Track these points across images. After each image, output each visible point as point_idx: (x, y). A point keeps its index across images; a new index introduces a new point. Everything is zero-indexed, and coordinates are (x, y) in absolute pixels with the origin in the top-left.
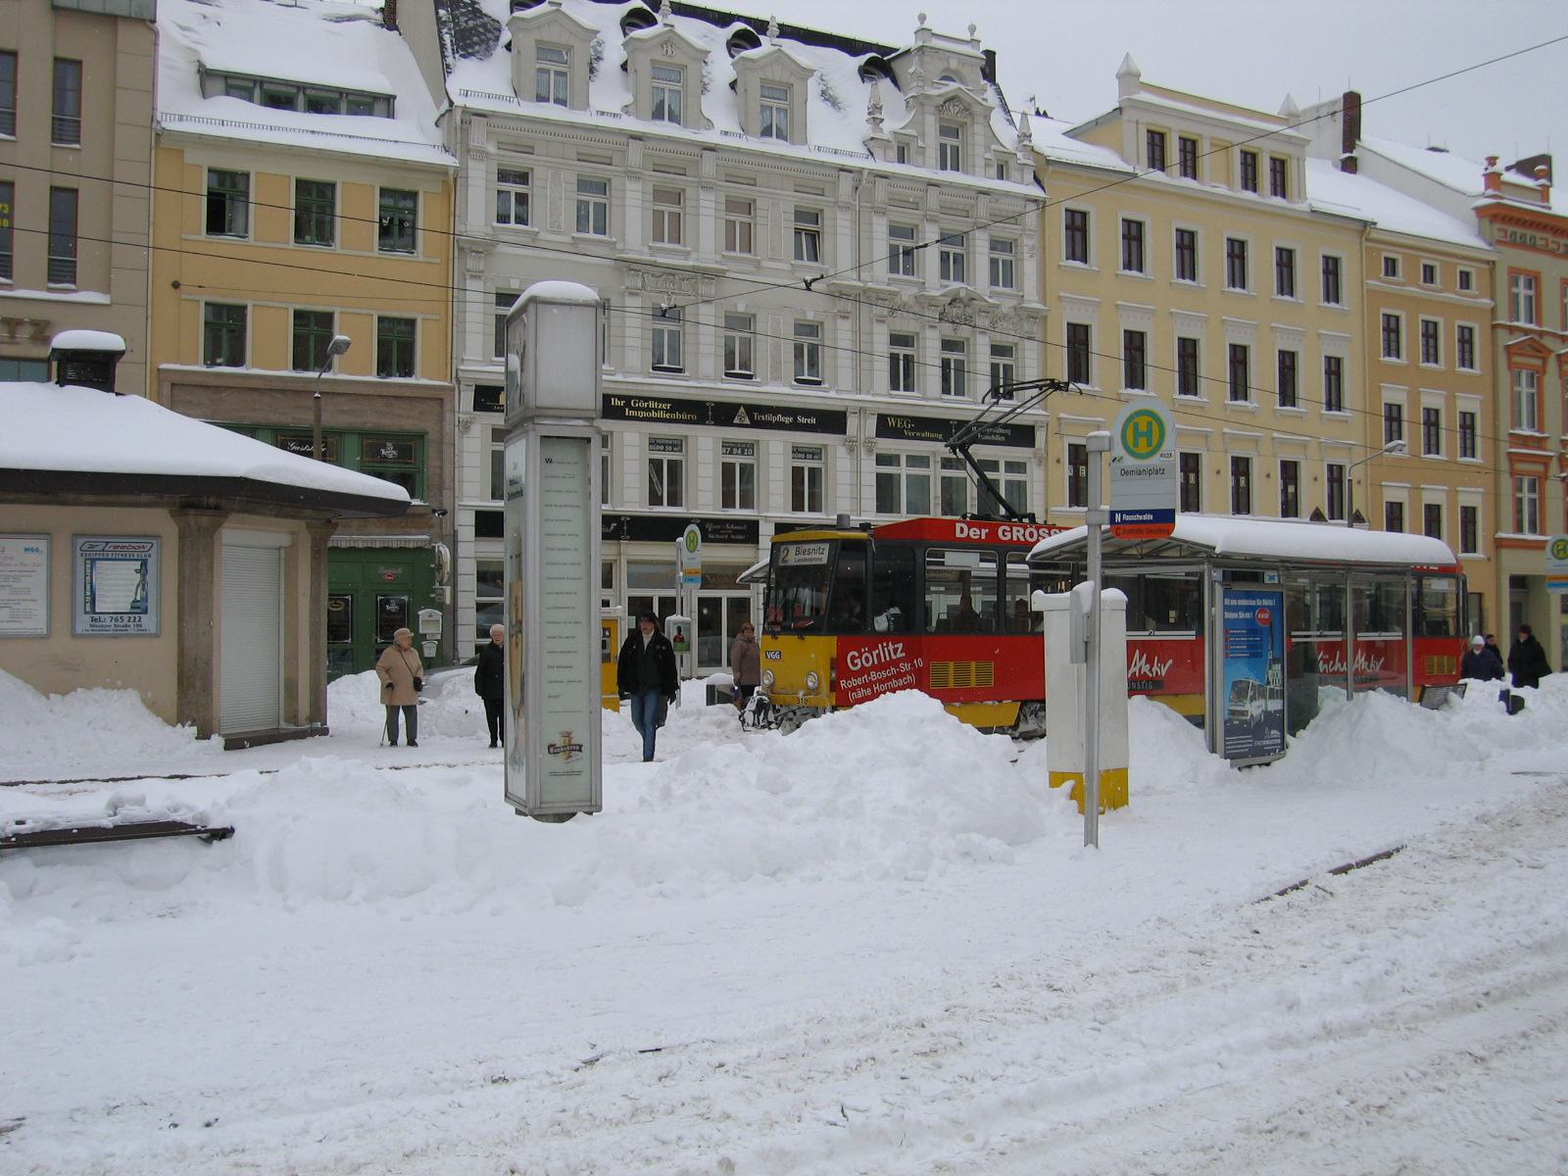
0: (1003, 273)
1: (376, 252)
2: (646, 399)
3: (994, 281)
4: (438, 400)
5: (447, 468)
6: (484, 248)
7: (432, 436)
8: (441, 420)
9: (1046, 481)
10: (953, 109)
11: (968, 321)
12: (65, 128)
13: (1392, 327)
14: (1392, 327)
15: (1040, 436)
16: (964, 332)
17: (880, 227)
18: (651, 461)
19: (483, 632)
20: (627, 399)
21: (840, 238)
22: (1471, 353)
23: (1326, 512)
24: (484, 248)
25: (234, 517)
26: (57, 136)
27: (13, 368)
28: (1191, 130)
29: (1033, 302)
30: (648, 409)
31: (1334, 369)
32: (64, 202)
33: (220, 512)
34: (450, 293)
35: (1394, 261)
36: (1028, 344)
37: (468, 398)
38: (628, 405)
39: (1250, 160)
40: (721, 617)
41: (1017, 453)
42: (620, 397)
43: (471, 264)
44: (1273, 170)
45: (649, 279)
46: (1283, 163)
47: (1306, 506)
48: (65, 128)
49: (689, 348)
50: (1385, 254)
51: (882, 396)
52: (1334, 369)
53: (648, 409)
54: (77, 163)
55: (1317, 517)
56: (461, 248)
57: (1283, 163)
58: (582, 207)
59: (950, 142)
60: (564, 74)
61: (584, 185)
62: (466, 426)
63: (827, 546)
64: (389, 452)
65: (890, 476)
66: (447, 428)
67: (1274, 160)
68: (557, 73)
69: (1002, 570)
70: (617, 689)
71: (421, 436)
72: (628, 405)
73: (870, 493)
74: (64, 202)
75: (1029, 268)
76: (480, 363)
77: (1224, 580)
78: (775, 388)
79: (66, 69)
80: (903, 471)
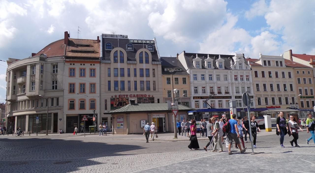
7: (189, 102)
8: (190, 100)
12: (154, 75)
13: (299, 80)
14: (299, 80)
19: (11, 113)
21: (192, 87)
22: (300, 81)
23: (292, 103)
26: (149, 82)
27: (312, 57)
28: (269, 60)
31: (291, 86)
34: (190, 87)
39: (277, 62)
44: (280, 63)
46: (281, 62)
47: (289, 103)
49: (229, 90)
51: (235, 94)
52: (291, 86)
54: (155, 79)
55: (291, 104)
57: (281, 62)
58: (202, 77)
63: (238, 113)
64: (185, 104)
65: (240, 103)
67: (280, 61)
69: (256, 113)
70: (299, 134)
71: (188, 102)
76: (193, 95)
77: (49, 114)
78: (223, 94)
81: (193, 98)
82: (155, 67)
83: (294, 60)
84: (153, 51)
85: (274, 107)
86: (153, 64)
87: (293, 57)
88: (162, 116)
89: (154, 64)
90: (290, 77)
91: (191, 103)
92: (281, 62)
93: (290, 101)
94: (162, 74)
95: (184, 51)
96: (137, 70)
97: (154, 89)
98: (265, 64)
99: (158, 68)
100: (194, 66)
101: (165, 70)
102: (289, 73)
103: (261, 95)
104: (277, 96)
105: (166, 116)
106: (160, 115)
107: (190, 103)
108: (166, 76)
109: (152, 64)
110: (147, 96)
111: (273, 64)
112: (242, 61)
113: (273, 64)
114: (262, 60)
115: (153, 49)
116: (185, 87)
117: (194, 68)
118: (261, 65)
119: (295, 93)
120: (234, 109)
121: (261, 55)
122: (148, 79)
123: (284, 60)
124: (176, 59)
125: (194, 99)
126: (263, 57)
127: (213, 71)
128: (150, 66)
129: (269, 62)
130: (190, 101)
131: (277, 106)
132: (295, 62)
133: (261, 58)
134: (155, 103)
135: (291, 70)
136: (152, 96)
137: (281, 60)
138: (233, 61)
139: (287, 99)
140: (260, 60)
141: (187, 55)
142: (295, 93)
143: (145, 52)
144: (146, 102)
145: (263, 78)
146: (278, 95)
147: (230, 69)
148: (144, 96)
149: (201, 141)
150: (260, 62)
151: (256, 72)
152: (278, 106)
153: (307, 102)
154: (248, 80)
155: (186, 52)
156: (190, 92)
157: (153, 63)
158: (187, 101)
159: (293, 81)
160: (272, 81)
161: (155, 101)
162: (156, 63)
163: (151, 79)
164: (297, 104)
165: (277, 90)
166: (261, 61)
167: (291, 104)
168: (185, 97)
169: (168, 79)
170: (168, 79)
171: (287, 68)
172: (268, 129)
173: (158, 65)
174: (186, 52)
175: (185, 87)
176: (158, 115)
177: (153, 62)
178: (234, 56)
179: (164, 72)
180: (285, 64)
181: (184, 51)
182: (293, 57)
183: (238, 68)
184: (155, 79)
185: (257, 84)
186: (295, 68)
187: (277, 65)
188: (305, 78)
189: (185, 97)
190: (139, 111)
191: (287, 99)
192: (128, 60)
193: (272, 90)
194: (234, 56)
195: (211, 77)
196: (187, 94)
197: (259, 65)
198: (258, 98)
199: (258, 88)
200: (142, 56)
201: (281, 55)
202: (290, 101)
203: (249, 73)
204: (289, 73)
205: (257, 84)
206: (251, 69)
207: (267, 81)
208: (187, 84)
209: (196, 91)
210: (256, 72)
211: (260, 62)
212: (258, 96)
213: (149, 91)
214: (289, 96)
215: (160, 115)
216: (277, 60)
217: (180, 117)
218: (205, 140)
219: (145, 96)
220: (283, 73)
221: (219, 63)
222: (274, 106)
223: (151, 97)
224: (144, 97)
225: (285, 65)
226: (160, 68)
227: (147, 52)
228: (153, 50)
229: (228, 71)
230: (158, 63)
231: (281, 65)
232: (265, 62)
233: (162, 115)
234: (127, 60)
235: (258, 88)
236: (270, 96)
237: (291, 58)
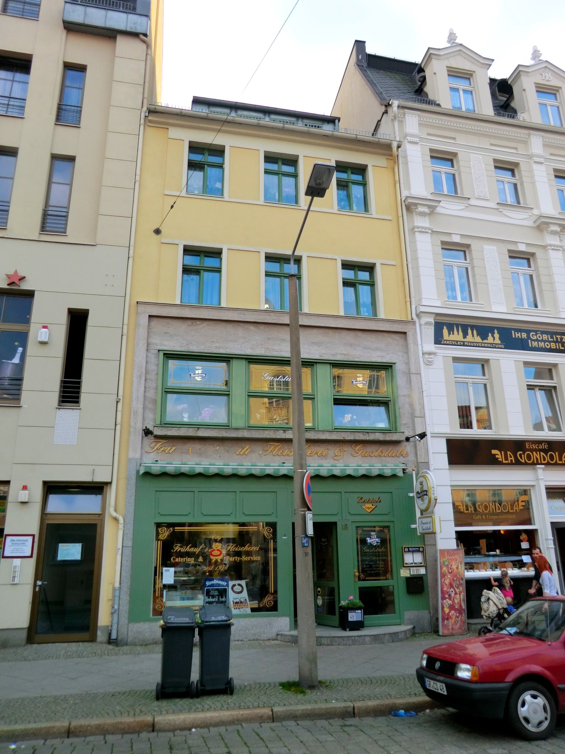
7: (399, 367)
38: (533, 336)
48: (67, 114)
81: (430, 332)
107: (408, 374)
125: (439, 340)
130: (408, 363)
161: (33, 327)
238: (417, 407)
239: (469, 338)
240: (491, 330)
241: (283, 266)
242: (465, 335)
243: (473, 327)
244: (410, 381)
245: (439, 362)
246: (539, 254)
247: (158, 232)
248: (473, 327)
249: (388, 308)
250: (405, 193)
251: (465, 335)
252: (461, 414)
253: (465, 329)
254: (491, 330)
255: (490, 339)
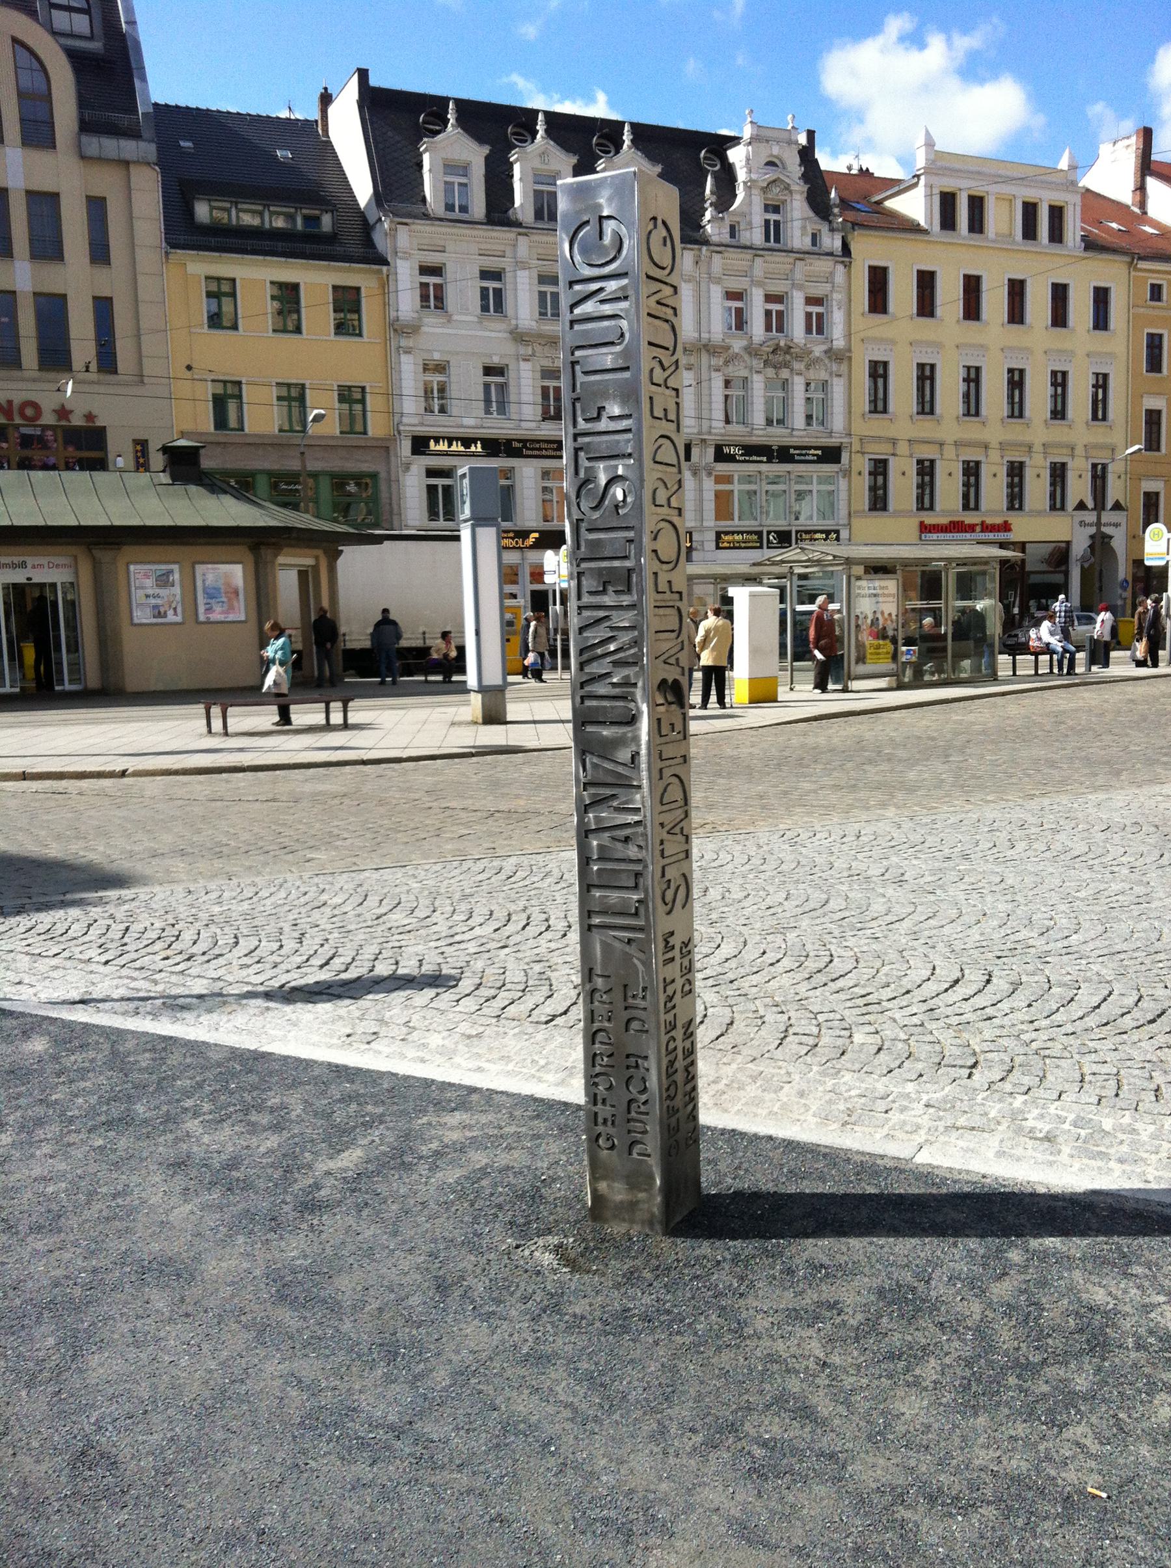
0: (817, 324)
1: (332, 337)
2: (538, 441)
3: (809, 330)
4: (385, 448)
5: (394, 498)
6: (413, 329)
7: (383, 475)
8: (388, 462)
9: (849, 490)
10: (776, 190)
11: (786, 365)
12: (100, 253)
15: (845, 457)
16: (785, 373)
17: (717, 292)
18: (540, 292)
20: (524, 441)
23: (1090, 505)
24: (413, 329)
25: (285, 550)
29: (839, 343)
30: (540, 449)
32: (103, 308)
33: (278, 548)
35: (1159, 287)
36: (836, 380)
37: (406, 446)
38: (525, 446)
40: (461, 593)
41: (828, 468)
42: (519, 441)
43: (404, 343)
45: (538, 348)
47: (1071, 503)
48: (100, 253)
50: (1150, 281)
52: (1101, 382)
53: (540, 449)
54: (111, 282)
55: (1081, 506)
56: (399, 329)
57: (981, 199)
58: (484, 292)
59: (773, 217)
60: (465, 185)
61: (485, 275)
62: (407, 467)
66: (393, 469)
68: (460, 184)
71: (374, 476)
72: (525, 446)
73: (710, 506)
74: (103, 308)
75: (837, 318)
79: (96, 207)
80: (736, 487)
82: (105, 182)
83: (1153, 211)
84: (96, 46)
85: (971, 528)
86: (91, 158)
87: (1151, 182)
88: (47, 570)
89: (100, 160)
90: (1101, 321)
91: (393, 482)
92: (1057, 213)
93: (1078, 488)
94: (168, 243)
95: (363, 74)
96: (1072, 295)
97: (107, 360)
98: (948, 221)
99: (135, 196)
100: (424, 200)
101: (202, 211)
102: (1101, 297)
103: (894, 442)
104: (998, 453)
105: (76, 573)
106: (34, 567)
107: (389, 480)
108: (202, 266)
109: (83, 157)
110: (48, 419)
111: (1001, 219)
112: (787, 188)
113: (1001, 219)
114: (929, 186)
115: (98, 30)
116: (354, 361)
117: (426, 216)
118: (922, 223)
119: (1116, 436)
120: (479, 530)
121: (930, 144)
122: (54, 279)
123: (1077, 199)
124: (311, 137)
126: (939, 164)
127: (832, 274)
128: (63, 173)
129: (977, 204)
130: (389, 472)
131: (989, 521)
132: (1155, 224)
133: (928, 171)
134: (111, 467)
135: (1110, 272)
136: (90, 417)
137: (1058, 198)
138: (727, 177)
139: (1058, 473)
140: (916, 185)
141: (378, 105)
142: (1116, 436)
143: (15, 40)
144: (37, 456)
145: (1097, 332)
146: (1003, 446)
147: (696, 242)
148: (23, 415)
149: (47, 784)
150: (913, 205)
151: (878, 279)
152: (998, 520)
153: (1147, 495)
154: (820, 331)
155: (374, 82)
156: (391, 394)
157: (93, 144)
158: (365, 467)
159: (1118, 350)
160: (1027, 349)
161: (111, 457)
162: (111, 146)
163: (75, 278)
164: (1117, 506)
165: (1005, 410)
166: (919, 192)
167: (1081, 506)
168: (354, 440)
169: (221, 292)
170: (221, 292)
171: (1089, 254)
172: (752, 681)
173: (132, 167)
174: (374, 82)
175: (354, 361)
176: (16, 560)
177: (85, 139)
178: (734, 141)
179: (183, 232)
180: (1079, 224)
181: (363, 74)
182: (1151, 182)
183: (757, 237)
184: (111, 282)
185: (874, 365)
186: (1142, 265)
187: (1030, 231)
188: (1161, 336)
189: (354, 440)
190: (203, 523)
191: (1058, 473)
192: (86, 126)
193: (1017, 410)
194: (734, 141)
195: (498, 293)
196: (369, 408)
197: (910, 228)
198: (875, 460)
199: (1017, 399)
200: (44, 87)
201: (1063, 164)
202: (1078, 488)
203: (829, 278)
204: (1101, 297)
205: (874, 365)
206: (846, 250)
207: (949, 341)
208: (365, 339)
209: (437, 397)
210: (878, 279)
211: (913, 205)
212: (871, 448)
213: (16, 373)
214: (1080, 450)
215: (30, 561)
216: (1031, 194)
217: (199, 583)
218: (123, 774)
219: (29, 412)
220: (1060, 293)
221: (531, 179)
222: (970, 518)
223: (77, 421)
224: (18, 420)
225: (1078, 239)
226: (146, 196)
227: (30, 42)
228: (91, 38)
229: (512, 236)
230: (129, 148)
231: (1056, 235)
232: (948, 201)
233: (44, 560)
234: (76, 128)
235: (1017, 399)
236: (950, 452)
237: (1141, 188)
238: (395, 507)
239: (454, 448)
240: (474, 441)
241: (294, 397)
242: (450, 445)
243: (457, 439)
244: (390, 487)
245: (414, 469)
246: (422, 411)
247: (189, 368)
248: (457, 439)
249: (376, 427)
250: (393, 314)
251: (450, 445)
252: (394, 486)
253: (450, 441)
254: (474, 441)
255: (473, 449)
